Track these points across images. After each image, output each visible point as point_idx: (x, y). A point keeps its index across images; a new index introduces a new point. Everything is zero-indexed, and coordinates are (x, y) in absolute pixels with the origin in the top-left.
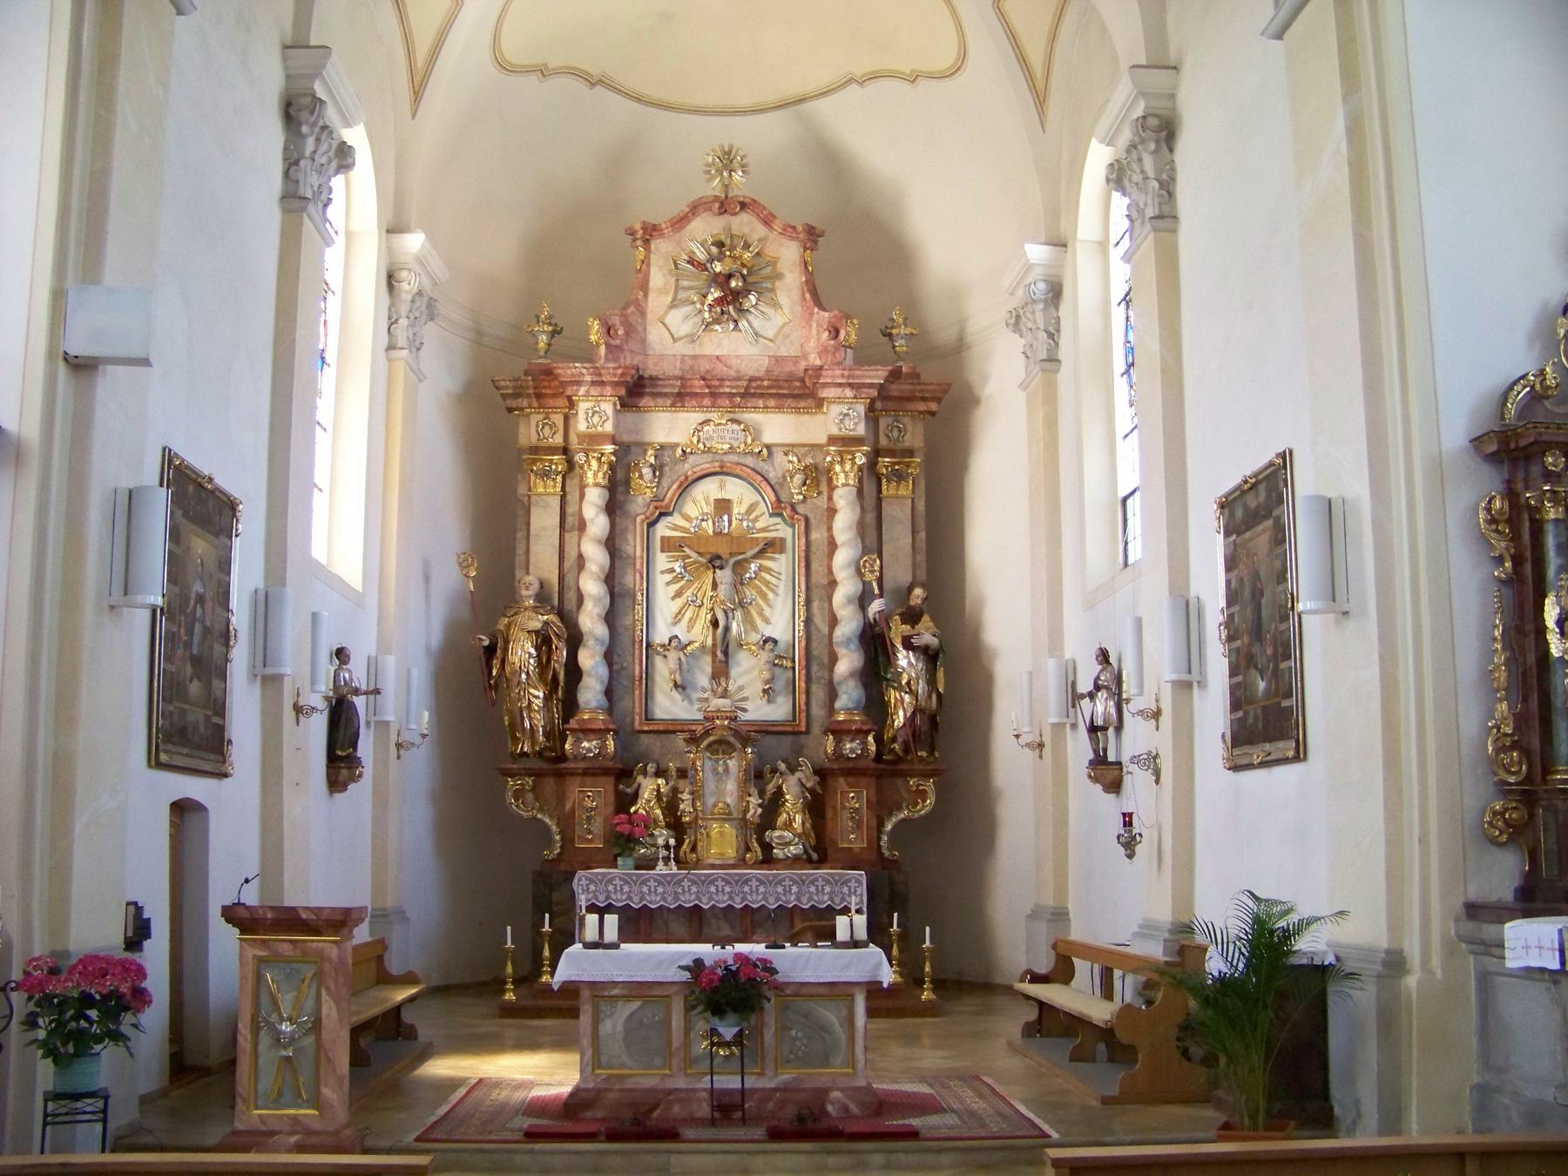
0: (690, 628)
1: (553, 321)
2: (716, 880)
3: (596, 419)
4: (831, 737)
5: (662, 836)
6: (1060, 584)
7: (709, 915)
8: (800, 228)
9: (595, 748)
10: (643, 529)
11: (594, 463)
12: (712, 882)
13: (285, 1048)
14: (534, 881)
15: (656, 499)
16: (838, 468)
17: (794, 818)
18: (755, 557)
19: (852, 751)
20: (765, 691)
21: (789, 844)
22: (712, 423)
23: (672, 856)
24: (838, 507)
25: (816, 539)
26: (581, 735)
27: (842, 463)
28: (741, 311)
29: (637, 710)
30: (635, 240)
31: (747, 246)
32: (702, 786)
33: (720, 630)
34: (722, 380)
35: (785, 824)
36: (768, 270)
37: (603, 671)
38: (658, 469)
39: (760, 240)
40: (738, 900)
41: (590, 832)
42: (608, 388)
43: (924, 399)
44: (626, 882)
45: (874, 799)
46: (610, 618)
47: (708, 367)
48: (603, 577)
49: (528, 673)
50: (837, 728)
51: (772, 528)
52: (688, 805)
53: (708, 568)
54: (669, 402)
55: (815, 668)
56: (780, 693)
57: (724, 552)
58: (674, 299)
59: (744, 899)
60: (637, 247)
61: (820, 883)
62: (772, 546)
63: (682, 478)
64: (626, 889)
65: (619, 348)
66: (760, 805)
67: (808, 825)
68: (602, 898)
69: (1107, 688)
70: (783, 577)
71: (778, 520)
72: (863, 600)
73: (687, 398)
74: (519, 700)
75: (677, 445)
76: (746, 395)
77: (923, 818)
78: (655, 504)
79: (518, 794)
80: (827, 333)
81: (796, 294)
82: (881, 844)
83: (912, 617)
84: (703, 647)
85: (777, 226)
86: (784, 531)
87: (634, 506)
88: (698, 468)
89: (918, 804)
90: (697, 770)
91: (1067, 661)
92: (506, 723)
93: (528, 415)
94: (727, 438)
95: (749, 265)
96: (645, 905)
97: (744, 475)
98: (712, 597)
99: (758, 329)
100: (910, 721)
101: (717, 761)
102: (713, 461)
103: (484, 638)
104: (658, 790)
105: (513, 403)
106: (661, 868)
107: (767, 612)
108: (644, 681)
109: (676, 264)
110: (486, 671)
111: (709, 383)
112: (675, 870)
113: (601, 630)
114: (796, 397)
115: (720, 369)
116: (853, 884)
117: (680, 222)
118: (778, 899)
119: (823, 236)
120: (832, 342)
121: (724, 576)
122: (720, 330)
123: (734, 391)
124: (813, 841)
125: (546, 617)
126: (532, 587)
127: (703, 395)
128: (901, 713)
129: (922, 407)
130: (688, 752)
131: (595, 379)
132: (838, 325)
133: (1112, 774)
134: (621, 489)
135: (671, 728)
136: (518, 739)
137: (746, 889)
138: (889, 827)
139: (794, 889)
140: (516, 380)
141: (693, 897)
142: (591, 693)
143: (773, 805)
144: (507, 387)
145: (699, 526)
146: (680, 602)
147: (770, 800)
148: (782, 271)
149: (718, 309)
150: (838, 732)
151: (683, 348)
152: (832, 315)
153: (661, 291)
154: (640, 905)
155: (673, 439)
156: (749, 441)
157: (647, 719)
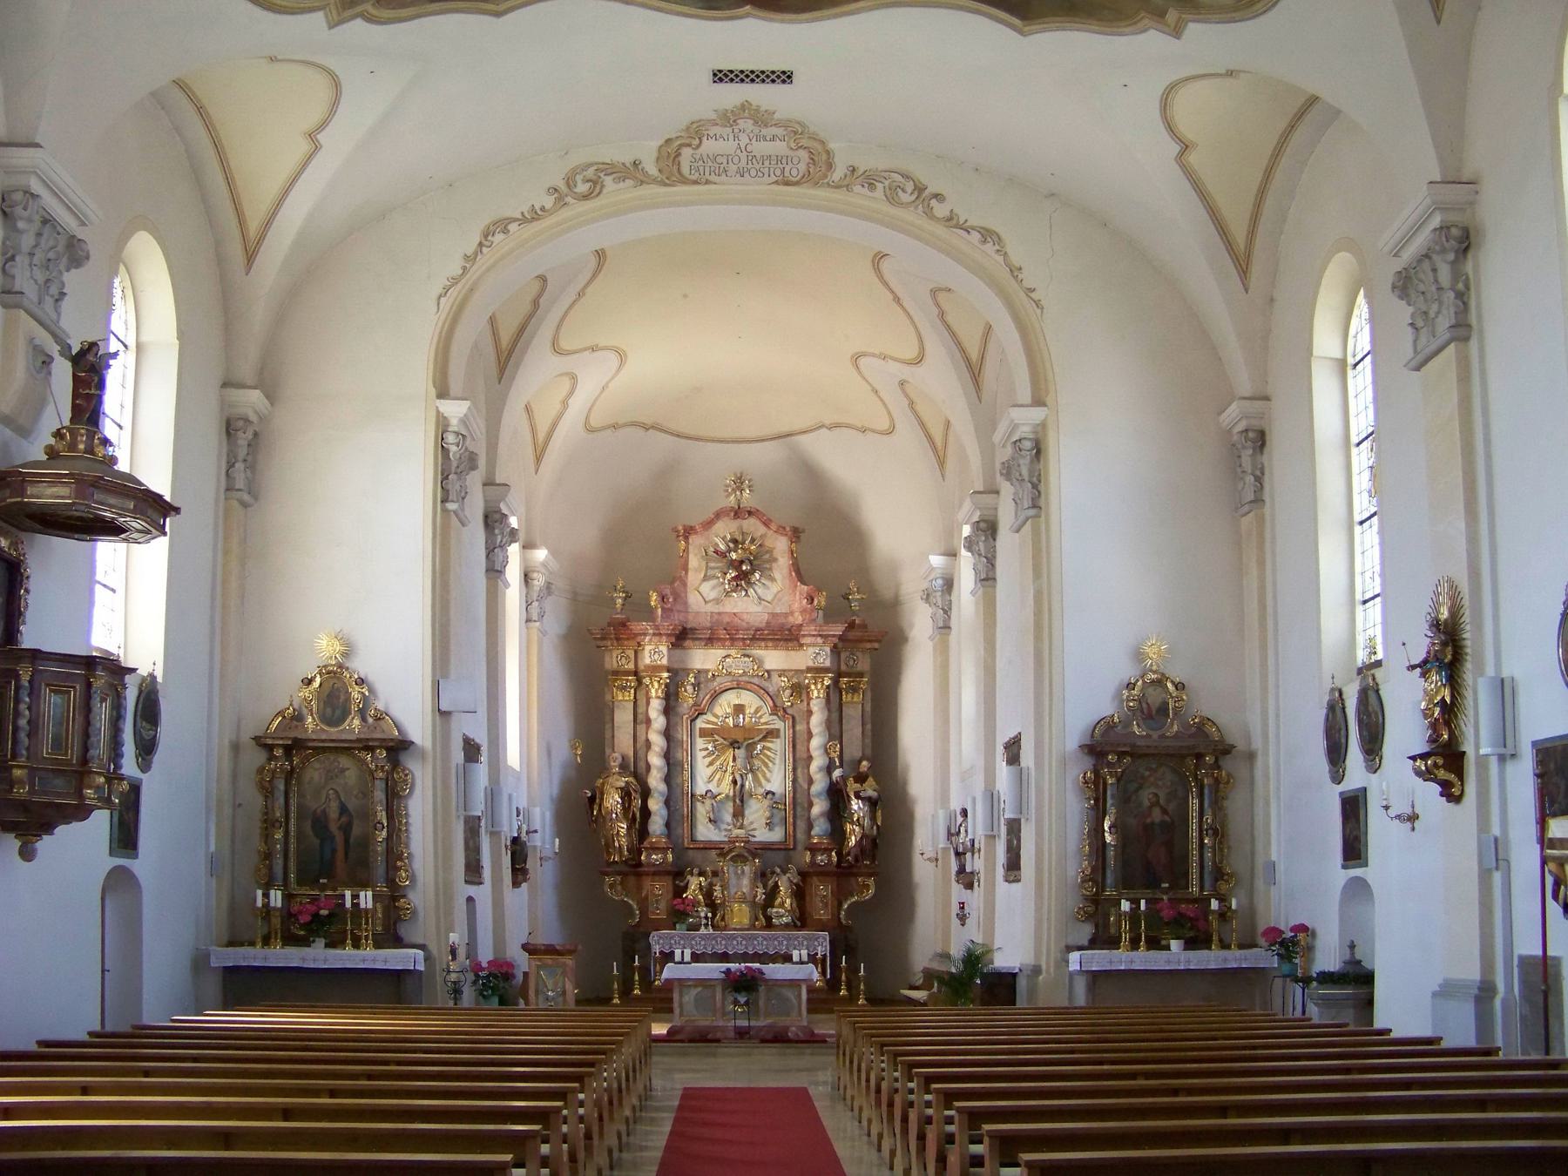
0: (720, 781)
3: (656, 656)
5: (703, 911)
8: (788, 529)
12: (734, 939)
15: (695, 704)
16: (813, 687)
18: (760, 741)
19: (822, 861)
21: (782, 916)
25: (800, 730)
27: (815, 684)
30: (678, 536)
33: (738, 786)
36: (767, 556)
37: (664, 812)
38: (696, 686)
43: (870, 641)
46: (668, 779)
48: (663, 754)
49: (616, 813)
54: (703, 644)
58: (705, 576)
62: (771, 734)
63: (713, 691)
66: (764, 894)
70: (778, 753)
71: (775, 717)
72: (829, 769)
76: (754, 639)
79: (611, 886)
81: (785, 571)
83: (861, 779)
84: (727, 796)
85: (774, 527)
86: (778, 724)
93: (611, 650)
100: (859, 843)
101: (737, 867)
104: (700, 884)
106: (703, 931)
107: (768, 775)
112: (711, 931)
113: (662, 787)
116: (821, 940)
117: (708, 524)
121: (741, 753)
124: (798, 915)
127: (725, 639)
128: (853, 838)
129: (868, 645)
131: (657, 632)
132: (813, 595)
134: (672, 698)
135: (707, 846)
137: (735, 942)
142: (657, 825)
143: (772, 893)
144: (598, 634)
146: (712, 768)
150: (813, 849)
151: (710, 608)
153: (697, 570)
155: (707, 667)
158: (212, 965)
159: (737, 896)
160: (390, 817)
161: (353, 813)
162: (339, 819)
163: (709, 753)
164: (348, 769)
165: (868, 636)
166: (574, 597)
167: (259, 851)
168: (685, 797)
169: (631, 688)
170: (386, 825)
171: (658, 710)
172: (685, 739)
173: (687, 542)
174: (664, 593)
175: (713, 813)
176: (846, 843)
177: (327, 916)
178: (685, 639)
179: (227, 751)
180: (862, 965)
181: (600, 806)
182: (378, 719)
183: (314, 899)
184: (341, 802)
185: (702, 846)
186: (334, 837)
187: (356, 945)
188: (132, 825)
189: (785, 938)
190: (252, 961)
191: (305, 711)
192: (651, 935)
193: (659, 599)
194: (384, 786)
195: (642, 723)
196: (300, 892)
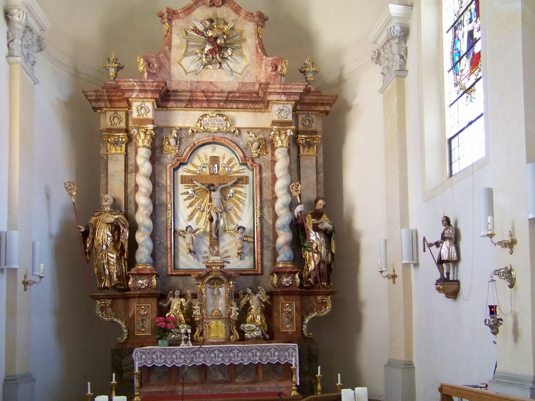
0: (198, 221)
2: (214, 350)
3: (143, 111)
4: (275, 275)
5: (184, 328)
6: (407, 190)
7: (211, 369)
11: (142, 135)
12: (212, 352)
14: (112, 354)
16: (277, 138)
17: (256, 317)
19: (287, 282)
20: (238, 253)
21: (254, 330)
22: (208, 116)
23: (189, 338)
24: (277, 158)
25: (266, 176)
26: (138, 277)
27: (280, 135)
28: (224, 58)
29: (169, 264)
31: (226, 23)
32: (206, 302)
33: (214, 223)
34: (213, 92)
35: (251, 320)
36: (238, 37)
37: (150, 243)
38: (178, 140)
39: (233, 21)
40: (227, 360)
42: (149, 94)
43: (323, 104)
44: (163, 353)
45: (299, 307)
46: (153, 216)
47: (205, 87)
48: (149, 195)
49: (107, 245)
50: (279, 271)
51: (241, 171)
53: (207, 192)
54: (184, 105)
55: (265, 242)
56: (247, 255)
57: (216, 183)
58: (186, 51)
59: (230, 360)
60: (164, 23)
62: (241, 181)
63: (192, 145)
64: (163, 357)
66: (238, 311)
67: (263, 321)
68: (149, 362)
69: (450, 239)
70: (247, 196)
71: (244, 167)
72: (291, 206)
73: (194, 103)
74: (102, 259)
75: (189, 128)
76: (227, 101)
77: (327, 315)
78: (177, 158)
79: (102, 309)
80: (271, 68)
81: (253, 50)
82: (303, 329)
83: (317, 215)
84: (205, 232)
85: (242, 14)
86: (247, 173)
88: (201, 140)
89: (322, 309)
90: (202, 293)
91: (412, 230)
92: (96, 272)
93: (105, 113)
94: (216, 124)
95: (227, 34)
96: (174, 365)
97: (226, 144)
98: (209, 206)
99: (232, 68)
100: (318, 266)
101: (214, 289)
102: (208, 136)
103: (81, 227)
104: (181, 305)
106: (183, 345)
107: (239, 214)
108: (173, 250)
109: (187, 33)
110: (83, 246)
111: (206, 94)
112: (191, 346)
113: (148, 222)
114: (254, 102)
115: (212, 88)
116: (291, 351)
117: (189, 10)
118: (249, 360)
119: (268, 20)
120: (274, 73)
121: (216, 195)
122: (212, 68)
123: (220, 99)
124: (266, 329)
125: (117, 216)
126: (108, 201)
127: (202, 101)
128: (313, 263)
129: (322, 108)
130: (197, 284)
131: (142, 88)
132: (277, 63)
133: (454, 287)
134: (158, 151)
136: (103, 280)
137: (232, 355)
138: (307, 321)
139: (258, 354)
141: (201, 360)
143: (245, 310)
144: (92, 96)
146: (192, 209)
147: (242, 308)
148: (245, 38)
149: (211, 56)
150: (280, 273)
151: (191, 78)
152: (274, 58)
153: (179, 47)
154: (171, 365)
155: (187, 125)
156: (229, 126)
157: (175, 269)
159: (213, 314)
165: (322, 100)
169: (123, 143)
171: (145, 157)
172: (168, 183)
175: (193, 245)
176: (306, 267)
178: (168, 101)
180: (339, 375)
181: (93, 240)
185: (183, 273)
189: (258, 350)
192: (135, 351)
195: (132, 172)
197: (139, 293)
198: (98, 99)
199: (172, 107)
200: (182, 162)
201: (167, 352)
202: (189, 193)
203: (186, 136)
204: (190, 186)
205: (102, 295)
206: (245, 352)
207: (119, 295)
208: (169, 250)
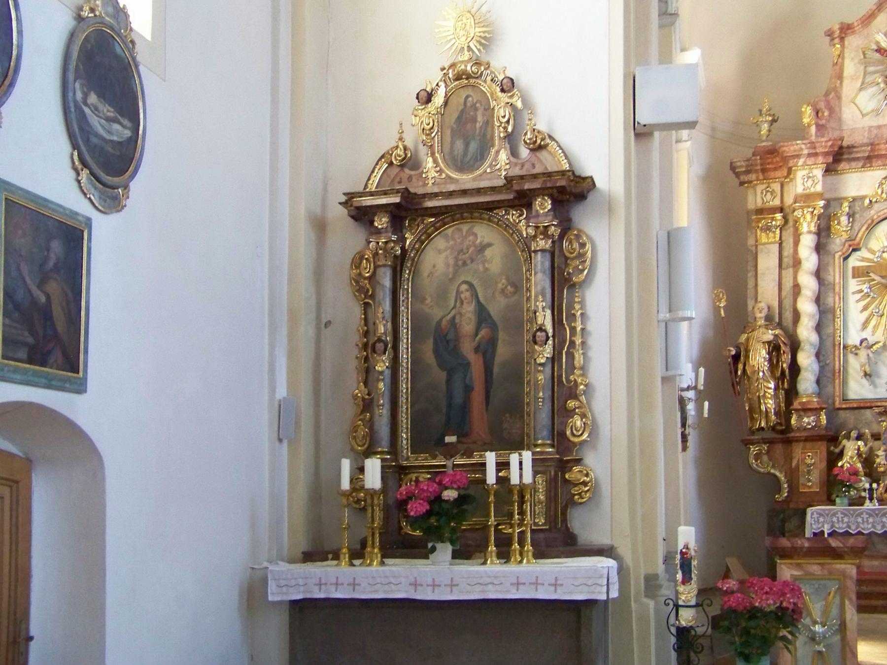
0: (874, 333)
1: (772, 112)
3: (810, 182)
9: (813, 422)
10: (840, 263)
13: (819, 644)
15: (850, 239)
26: (802, 413)
29: (837, 394)
30: (833, 39)
37: (816, 367)
38: (851, 215)
41: (809, 481)
44: (846, 515)
48: (814, 299)
49: (763, 372)
52: (882, 459)
54: (861, 164)
58: (863, 83)
61: (840, 515)
63: (870, 222)
64: (846, 520)
65: (823, 126)
74: (758, 391)
78: (850, 243)
87: (833, 246)
88: (882, 213)
93: (754, 187)
104: (859, 449)
105: (744, 178)
106: (868, 505)
112: (877, 506)
113: (814, 338)
126: (763, 311)
134: (823, 234)
135: (862, 405)
137: (860, 520)
140: (748, 160)
142: (807, 384)
144: (741, 166)
145: (881, 257)
146: (866, 314)
153: (853, 78)
154: (856, 532)
158: (270, 598)
160: (557, 322)
161: (499, 324)
162: (476, 335)
163: (862, 296)
164: (489, 245)
166: (713, 133)
167: (355, 397)
168: (837, 348)
170: (550, 334)
171: (810, 247)
172: (837, 280)
173: (843, 46)
174: (818, 107)
175: (869, 365)
177: (455, 500)
179: (305, 234)
182: (538, 148)
183: (437, 473)
184: (479, 302)
185: (855, 406)
186: (468, 364)
187: (504, 555)
188: (58, 312)
190: (333, 588)
191: (423, 150)
193: (813, 114)
194: (547, 264)
195: (787, 267)
196: (417, 463)
197: (806, 435)
198: (749, 170)
199: (843, 170)
200: (855, 247)
201: (850, 513)
202: (863, 291)
203: (861, 210)
204: (865, 280)
205: (758, 439)
206: (877, 517)
207: (779, 438)
208: (837, 374)
